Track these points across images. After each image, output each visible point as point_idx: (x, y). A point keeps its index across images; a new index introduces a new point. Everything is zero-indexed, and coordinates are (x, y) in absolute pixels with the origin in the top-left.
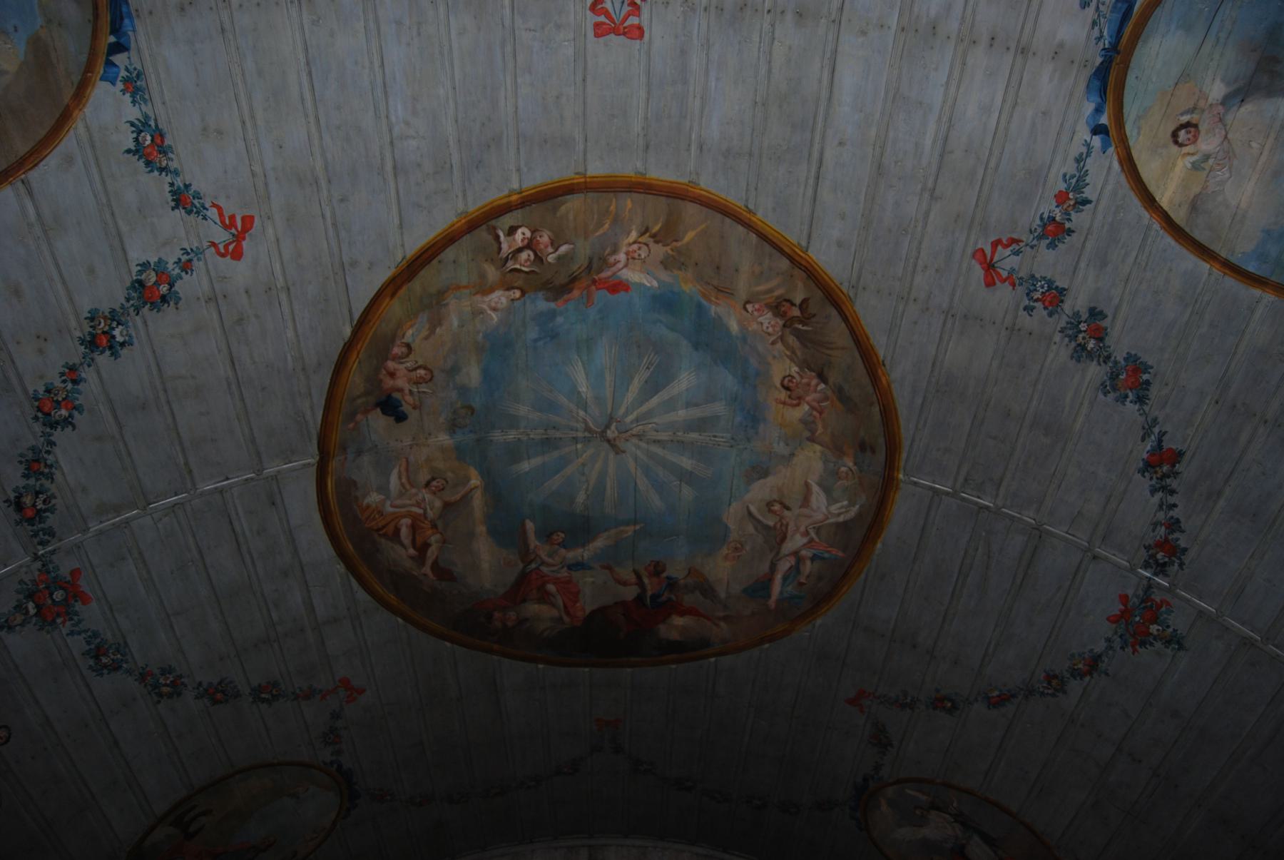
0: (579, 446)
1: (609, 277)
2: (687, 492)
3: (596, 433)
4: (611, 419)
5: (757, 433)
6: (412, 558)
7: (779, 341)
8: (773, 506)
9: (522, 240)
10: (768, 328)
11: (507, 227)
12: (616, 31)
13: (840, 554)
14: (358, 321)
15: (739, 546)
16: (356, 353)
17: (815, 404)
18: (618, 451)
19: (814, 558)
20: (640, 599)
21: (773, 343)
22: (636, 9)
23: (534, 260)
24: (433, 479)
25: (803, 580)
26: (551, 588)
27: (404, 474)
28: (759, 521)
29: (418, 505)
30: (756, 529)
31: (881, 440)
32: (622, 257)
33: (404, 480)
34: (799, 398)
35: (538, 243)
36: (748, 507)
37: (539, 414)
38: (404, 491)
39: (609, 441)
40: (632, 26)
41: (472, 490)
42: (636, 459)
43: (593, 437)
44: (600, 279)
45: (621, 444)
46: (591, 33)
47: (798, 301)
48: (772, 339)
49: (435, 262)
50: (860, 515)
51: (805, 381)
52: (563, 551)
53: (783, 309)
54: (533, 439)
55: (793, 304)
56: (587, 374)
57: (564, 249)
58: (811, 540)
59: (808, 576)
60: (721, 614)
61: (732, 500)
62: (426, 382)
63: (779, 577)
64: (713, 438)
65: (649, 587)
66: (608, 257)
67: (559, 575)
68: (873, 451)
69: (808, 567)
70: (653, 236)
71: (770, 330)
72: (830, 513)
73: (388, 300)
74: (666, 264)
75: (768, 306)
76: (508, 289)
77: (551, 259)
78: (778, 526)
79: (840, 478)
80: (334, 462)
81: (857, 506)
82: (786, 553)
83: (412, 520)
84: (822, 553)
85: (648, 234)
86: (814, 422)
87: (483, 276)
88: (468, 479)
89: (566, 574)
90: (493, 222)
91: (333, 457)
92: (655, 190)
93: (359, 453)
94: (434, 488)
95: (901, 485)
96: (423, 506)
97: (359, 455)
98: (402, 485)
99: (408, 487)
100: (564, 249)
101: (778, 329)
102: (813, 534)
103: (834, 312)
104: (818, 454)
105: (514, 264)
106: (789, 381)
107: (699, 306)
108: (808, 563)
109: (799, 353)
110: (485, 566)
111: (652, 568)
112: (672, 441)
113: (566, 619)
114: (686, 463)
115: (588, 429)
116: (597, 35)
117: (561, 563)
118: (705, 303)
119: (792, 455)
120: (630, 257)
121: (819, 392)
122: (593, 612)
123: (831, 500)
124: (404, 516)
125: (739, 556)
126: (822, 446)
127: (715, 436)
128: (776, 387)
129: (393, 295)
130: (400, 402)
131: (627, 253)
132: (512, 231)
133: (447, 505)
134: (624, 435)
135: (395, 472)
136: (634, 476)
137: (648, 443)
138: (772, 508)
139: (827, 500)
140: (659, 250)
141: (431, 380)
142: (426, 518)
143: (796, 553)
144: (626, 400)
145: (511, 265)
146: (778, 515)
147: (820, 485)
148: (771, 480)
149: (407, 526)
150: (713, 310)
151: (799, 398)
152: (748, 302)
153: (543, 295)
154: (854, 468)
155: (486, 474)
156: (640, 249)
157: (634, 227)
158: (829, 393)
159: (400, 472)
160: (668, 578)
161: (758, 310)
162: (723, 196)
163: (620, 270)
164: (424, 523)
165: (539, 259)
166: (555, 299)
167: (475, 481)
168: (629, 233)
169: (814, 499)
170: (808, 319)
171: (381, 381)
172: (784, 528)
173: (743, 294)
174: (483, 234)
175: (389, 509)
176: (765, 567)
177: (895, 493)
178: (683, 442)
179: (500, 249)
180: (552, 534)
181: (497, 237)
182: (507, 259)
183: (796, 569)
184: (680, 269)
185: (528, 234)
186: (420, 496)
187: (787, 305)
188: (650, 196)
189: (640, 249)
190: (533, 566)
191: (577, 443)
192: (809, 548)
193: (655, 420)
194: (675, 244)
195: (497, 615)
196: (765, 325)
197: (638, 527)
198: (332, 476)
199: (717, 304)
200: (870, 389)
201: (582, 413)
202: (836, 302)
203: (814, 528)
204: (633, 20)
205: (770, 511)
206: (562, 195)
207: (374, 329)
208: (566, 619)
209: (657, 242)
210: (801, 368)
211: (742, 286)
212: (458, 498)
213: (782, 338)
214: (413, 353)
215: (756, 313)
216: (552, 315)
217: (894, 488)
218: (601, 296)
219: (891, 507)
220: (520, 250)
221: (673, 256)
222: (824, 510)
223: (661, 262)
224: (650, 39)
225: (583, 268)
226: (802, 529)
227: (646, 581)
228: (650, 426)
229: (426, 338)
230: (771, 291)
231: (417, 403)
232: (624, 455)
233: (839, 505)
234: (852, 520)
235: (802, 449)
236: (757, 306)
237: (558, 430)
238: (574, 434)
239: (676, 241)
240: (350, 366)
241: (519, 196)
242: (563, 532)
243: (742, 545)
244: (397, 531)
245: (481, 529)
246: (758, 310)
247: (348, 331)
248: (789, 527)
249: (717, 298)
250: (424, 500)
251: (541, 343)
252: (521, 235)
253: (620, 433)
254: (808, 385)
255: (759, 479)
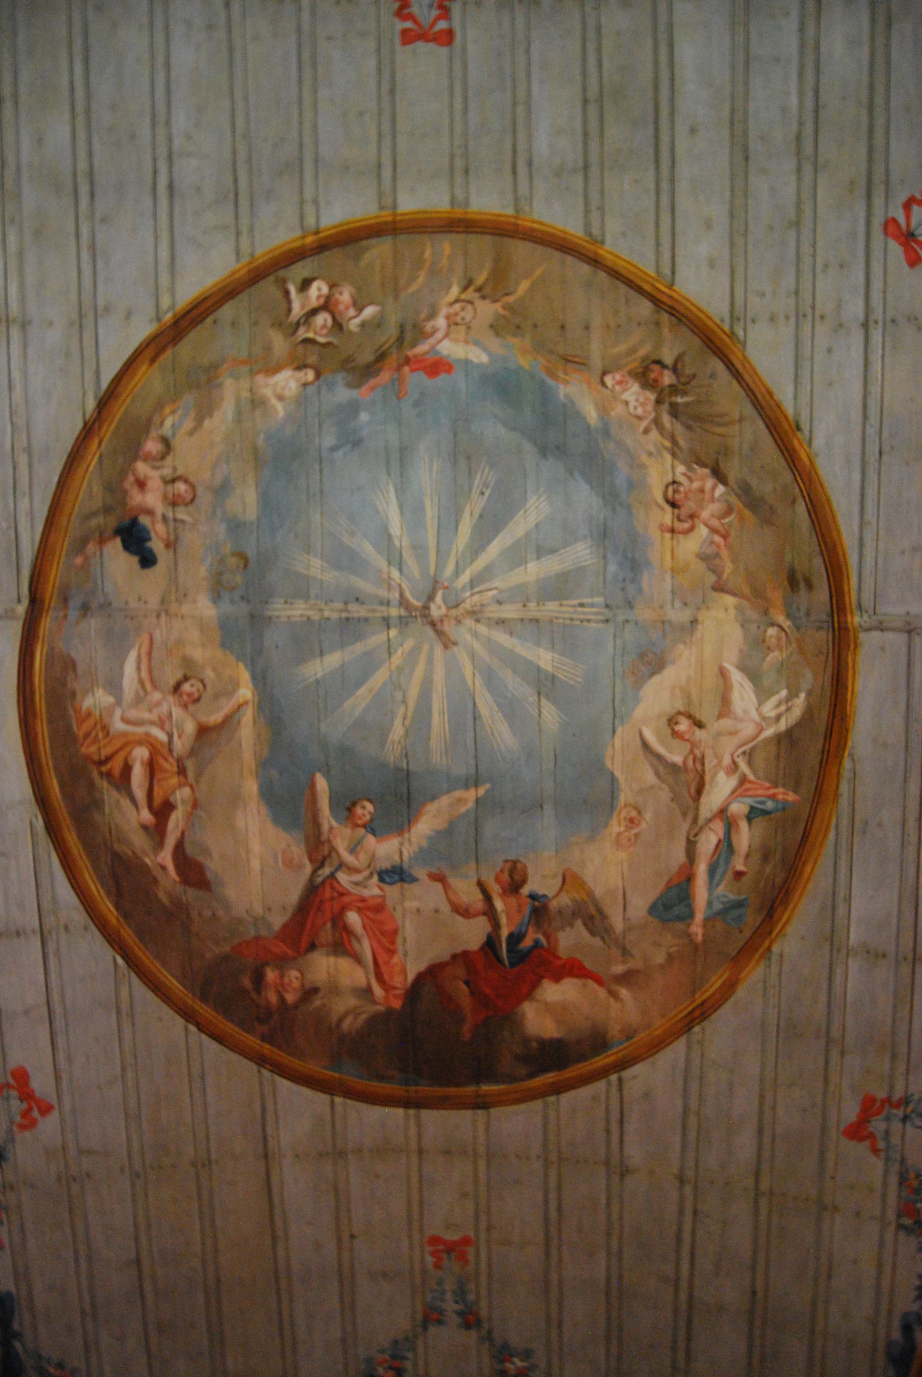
0: (393, 633)
1: (426, 353)
2: (550, 714)
3: (416, 609)
4: (435, 585)
5: (640, 590)
6: (145, 827)
7: (653, 427)
8: (676, 723)
9: (319, 297)
10: (635, 408)
11: (299, 279)
12: (424, 36)
13: (791, 797)
14: (106, 391)
15: (634, 814)
16: (96, 441)
17: (715, 523)
18: (448, 643)
19: (753, 814)
20: (491, 944)
21: (646, 431)
22: (445, 12)
23: (333, 326)
24: (186, 679)
25: (740, 867)
26: (353, 918)
27: (144, 661)
28: (659, 757)
29: (161, 724)
30: (657, 774)
31: (818, 561)
32: (441, 322)
33: (144, 674)
34: (692, 516)
35: (337, 303)
36: (641, 734)
37: (336, 573)
38: (142, 693)
39: (433, 624)
40: (441, 31)
41: (239, 707)
42: (473, 656)
43: (411, 616)
44: (415, 356)
45: (447, 627)
46: (398, 41)
47: (668, 360)
48: (645, 423)
49: (209, 320)
50: (809, 713)
51: (696, 485)
52: (371, 839)
53: (652, 375)
54: (328, 619)
55: (664, 366)
56: (401, 507)
57: (369, 311)
58: (743, 780)
59: (747, 856)
60: (619, 969)
61: (616, 723)
62: (186, 505)
63: (702, 869)
64: (579, 609)
65: (503, 920)
66: (425, 323)
67: (366, 893)
68: (809, 586)
69: (744, 837)
70: (479, 290)
71: (640, 411)
72: (764, 718)
73: (144, 368)
74: (496, 328)
75: (634, 374)
76: (299, 368)
77: (353, 325)
78: (690, 763)
79: (769, 648)
80: (48, 619)
81: (802, 696)
82: (709, 815)
83: (151, 754)
84: (763, 803)
85: (471, 289)
86: (717, 555)
87: (268, 348)
88: (236, 686)
89: (376, 891)
90: (282, 273)
91: (48, 610)
92: (480, 227)
93: (85, 609)
94: (185, 697)
95: (862, 636)
96: (167, 726)
97: (85, 615)
98: (141, 682)
99: (148, 686)
100: (369, 311)
101: (649, 408)
102: (743, 766)
103: (720, 366)
104: (732, 612)
105: (307, 331)
106: (675, 492)
107: (542, 384)
108: (744, 825)
109: (682, 442)
110: (255, 864)
111: (506, 877)
112: (522, 620)
113: (378, 991)
114: (545, 659)
115: (403, 602)
116: (404, 43)
117: (369, 866)
118: (550, 382)
119: (694, 622)
120: (452, 323)
121: (719, 500)
122: (421, 978)
123: (763, 694)
124: (140, 743)
125: (636, 835)
126: (734, 594)
127: (582, 605)
128: (658, 506)
129: (153, 360)
130: (148, 532)
131: (448, 317)
132: (305, 285)
133: (203, 731)
134: (453, 612)
135: (132, 656)
136: (472, 689)
137: (489, 626)
138: (677, 728)
139: (757, 696)
140: (487, 310)
141: (192, 501)
142: (171, 751)
143: (722, 812)
144: (454, 552)
145: (302, 333)
146: (688, 740)
147: (742, 668)
148: (669, 674)
149: (142, 762)
150: (562, 391)
151: (692, 516)
152: (604, 373)
153: (343, 379)
154: (786, 624)
155: (260, 679)
156: (463, 309)
157: (455, 280)
158: (734, 500)
159: (139, 656)
160: (533, 897)
161: (620, 383)
162: (561, 227)
163: (440, 341)
164: (166, 759)
165: (338, 326)
166: (358, 386)
167: (246, 692)
168: (449, 287)
169: (735, 696)
170: (688, 383)
171: (125, 492)
172: (699, 767)
173: (597, 362)
174: (268, 287)
175: (118, 725)
176: (680, 856)
177: (855, 654)
178: (537, 620)
179: (289, 310)
180: (354, 804)
181: (287, 293)
182: (298, 325)
183: (727, 846)
184: (515, 335)
185: (325, 290)
186: (164, 708)
187: (656, 367)
188: (471, 236)
189: (463, 309)
190: (326, 871)
191: (389, 628)
192: (741, 795)
193: (497, 583)
194: (506, 299)
195: (271, 975)
196: (632, 404)
197: (481, 792)
198: (43, 643)
199: (566, 383)
200: (788, 476)
201: (395, 574)
202: (719, 349)
203: (744, 753)
204: (442, 25)
205: (676, 734)
206: (366, 238)
207: (123, 408)
208: (378, 991)
209: (483, 297)
210: (689, 468)
211: (596, 352)
212: (220, 720)
213: (657, 422)
214: (172, 453)
215: (618, 388)
216: (353, 408)
217: (852, 647)
218: (416, 380)
219: (853, 684)
220: (314, 312)
221: (504, 317)
222: (754, 714)
223: (491, 326)
224: (740, 747)
225: (391, 341)
226: (727, 761)
227: (499, 905)
228: (490, 594)
229: (191, 433)
230: (633, 350)
231: (172, 537)
232: (455, 649)
233: (774, 700)
234: (799, 724)
235: (708, 608)
236: (618, 377)
237: (362, 603)
238: (382, 611)
239: (507, 294)
240: (88, 461)
241: (316, 237)
242: (370, 801)
243: (640, 813)
244: (127, 769)
245: (251, 787)
246: (620, 383)
247: (91, 405)
248: (706, 762)
249: (566, 373)
250: (170, 715)
251: (339, 454)
252: (318, 290)
253: (449, 608)
254: (702, 491)
255: (652, 674)
